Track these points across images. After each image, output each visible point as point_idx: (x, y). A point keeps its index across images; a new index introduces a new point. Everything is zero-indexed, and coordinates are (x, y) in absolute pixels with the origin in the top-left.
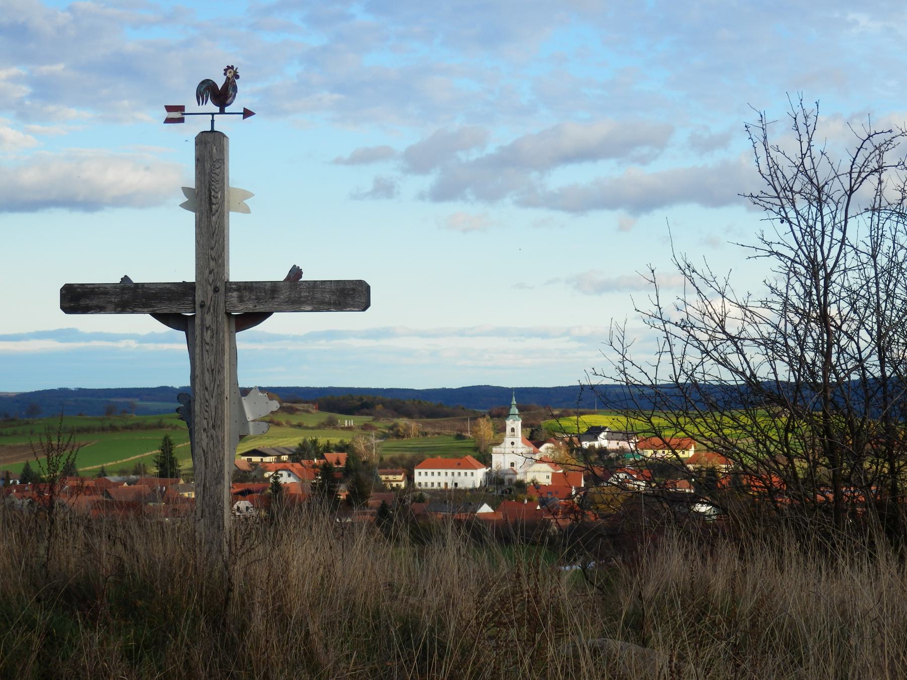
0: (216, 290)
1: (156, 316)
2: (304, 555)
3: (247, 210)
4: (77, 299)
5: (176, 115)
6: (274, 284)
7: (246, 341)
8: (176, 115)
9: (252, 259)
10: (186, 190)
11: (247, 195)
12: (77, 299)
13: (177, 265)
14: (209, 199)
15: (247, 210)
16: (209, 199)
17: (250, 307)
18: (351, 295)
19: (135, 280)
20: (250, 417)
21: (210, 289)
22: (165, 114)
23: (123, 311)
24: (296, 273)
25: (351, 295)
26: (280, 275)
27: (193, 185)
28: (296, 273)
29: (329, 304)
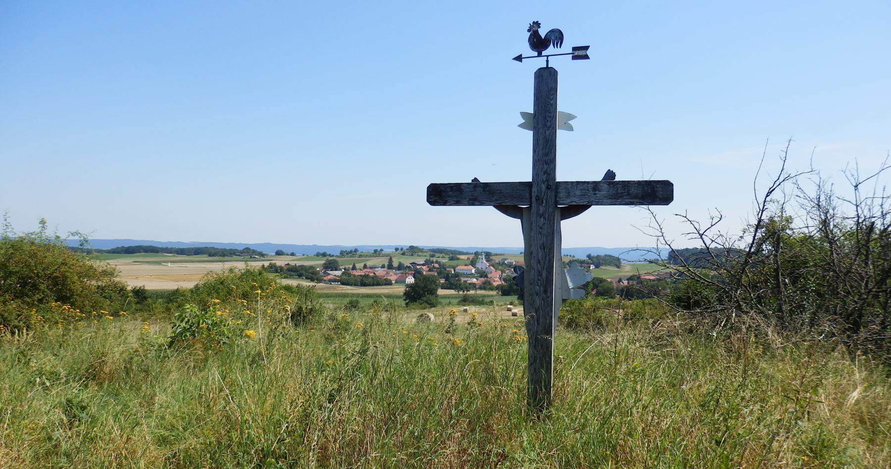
0: (548, 187)
1: (496, 207)
2: (71, 238)
3: (571, 129)
4: (440, 194)
5: (581, 53)
6: (595, 183)
7: (568, 226)
8: (581, 53)
9: (574, 165)
10: (524, 115)
11: (572, 117)
12: (440, 194)
13: (521, 170)
14: (544, 121)
15: (571, 129)
16: (544, 121)
17: (575, 201)
18: (656, 193)
19: (483, 180)
20: (571, 285)
21: (544, 187)
22: (589, 52)
23: (473, 204)
24: (610, 175)
25: (656, 193)
26: (599, 177)
27: (531, 110)
28: (610, 175)
29: (636, 197)
